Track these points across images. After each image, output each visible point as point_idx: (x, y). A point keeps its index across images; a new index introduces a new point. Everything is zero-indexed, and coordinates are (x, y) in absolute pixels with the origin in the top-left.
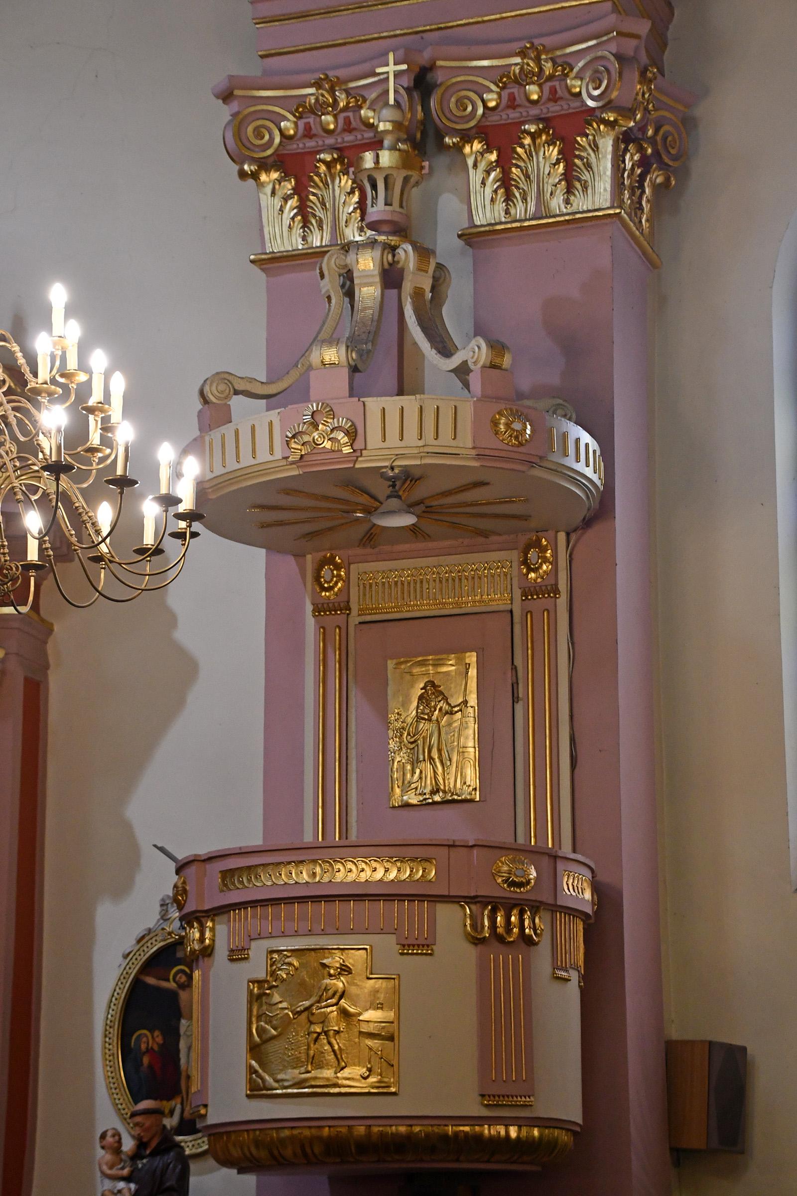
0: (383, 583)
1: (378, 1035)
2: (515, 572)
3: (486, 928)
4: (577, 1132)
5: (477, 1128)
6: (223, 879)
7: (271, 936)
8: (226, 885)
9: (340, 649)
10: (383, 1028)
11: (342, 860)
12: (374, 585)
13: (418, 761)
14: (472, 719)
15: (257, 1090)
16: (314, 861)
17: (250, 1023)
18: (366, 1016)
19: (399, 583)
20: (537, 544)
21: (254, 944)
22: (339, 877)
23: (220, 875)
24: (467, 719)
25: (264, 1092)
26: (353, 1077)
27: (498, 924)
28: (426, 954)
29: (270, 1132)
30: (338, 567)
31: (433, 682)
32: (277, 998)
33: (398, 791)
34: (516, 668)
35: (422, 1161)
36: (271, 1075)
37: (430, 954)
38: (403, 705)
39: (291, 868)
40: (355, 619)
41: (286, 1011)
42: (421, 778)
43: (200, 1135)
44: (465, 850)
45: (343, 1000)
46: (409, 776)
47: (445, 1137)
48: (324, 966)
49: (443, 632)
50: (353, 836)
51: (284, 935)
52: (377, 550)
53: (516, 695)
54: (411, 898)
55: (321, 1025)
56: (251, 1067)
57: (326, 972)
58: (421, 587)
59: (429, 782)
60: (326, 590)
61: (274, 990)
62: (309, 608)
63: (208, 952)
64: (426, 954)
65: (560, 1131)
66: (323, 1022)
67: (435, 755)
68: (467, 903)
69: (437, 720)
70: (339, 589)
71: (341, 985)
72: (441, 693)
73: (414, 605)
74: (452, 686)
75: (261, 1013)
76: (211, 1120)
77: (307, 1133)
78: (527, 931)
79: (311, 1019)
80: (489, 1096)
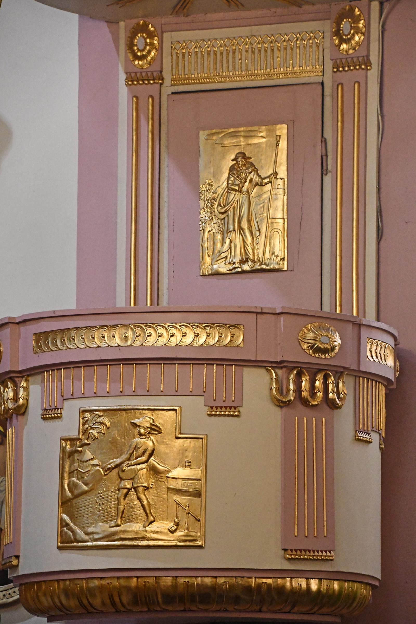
0: (196, 53)
1: (186, 491)
2: (327, 43)
3: (291, 392)
4: (376, 586)
5: (279, 581)
6: (37, 341)
7: (84, 397)
8: (39, 347)
9: (153, 119)
10: (191, 485)
11: (154, 325)
12: (187, 55)
13: (228, 231)
14: (281, 191)
15: (67, 542)
16: (126, 326)
17: (62, 478)
18: (174, 473)
19: (212, 54)
20: (350, 14)
21: (67, 404)
22: (151, 341)
23: (34, 338)
24: (277, 191)
25: (75, 544)
26: (161, 530)
27: (303, 388)
28: (233, 416)
29: (79, 582)
30: (151, 35)
31: (244, 154)
32: (88, 455)
33: (208, 260)
34: (325, 140)
35: (226, 611)
36: (82, 528)
37: (237, 416)
38: (214, 176)
39: (104, 332)
40: (167, 89)
41: (98, 468)
42: (230, 248)
43: (11, 585)
44: (273, 317)
45: (152, 458)
46: (219, 245)
47: (248, 589)
48: (135, 425)
49: (253, 104)
50: (164, 303)
51: (96, 395)
52: (190, 18)
53: (325, 168)
54: (220, 362)
55: (131, 482)
56: (62, 520)
57: (136, 431)
58: (234, 58)
59: (238, 252)
60: (140, 58)
61: (86, 447)
62: (123, 77)
63: (21, 411)
64: (233, 416)
65: (359, 585)
66: (132, 479)
67: (245, 225)
68: (273, 368)
69: (247, 191)
70: (152, 58)
71: (150, 444)
72: (252, 165)
73: (226, 77)
74: (263, 157)
75: (73, 469)
76: (22, 571)
77: (116, 583)
78: (331, 395)
79: (122, 475)
80: (292, 550)
